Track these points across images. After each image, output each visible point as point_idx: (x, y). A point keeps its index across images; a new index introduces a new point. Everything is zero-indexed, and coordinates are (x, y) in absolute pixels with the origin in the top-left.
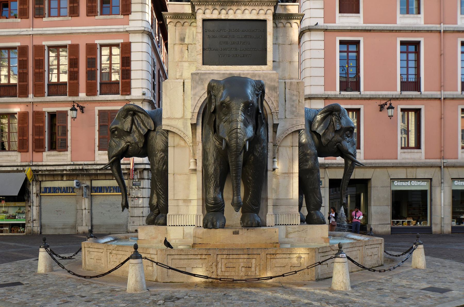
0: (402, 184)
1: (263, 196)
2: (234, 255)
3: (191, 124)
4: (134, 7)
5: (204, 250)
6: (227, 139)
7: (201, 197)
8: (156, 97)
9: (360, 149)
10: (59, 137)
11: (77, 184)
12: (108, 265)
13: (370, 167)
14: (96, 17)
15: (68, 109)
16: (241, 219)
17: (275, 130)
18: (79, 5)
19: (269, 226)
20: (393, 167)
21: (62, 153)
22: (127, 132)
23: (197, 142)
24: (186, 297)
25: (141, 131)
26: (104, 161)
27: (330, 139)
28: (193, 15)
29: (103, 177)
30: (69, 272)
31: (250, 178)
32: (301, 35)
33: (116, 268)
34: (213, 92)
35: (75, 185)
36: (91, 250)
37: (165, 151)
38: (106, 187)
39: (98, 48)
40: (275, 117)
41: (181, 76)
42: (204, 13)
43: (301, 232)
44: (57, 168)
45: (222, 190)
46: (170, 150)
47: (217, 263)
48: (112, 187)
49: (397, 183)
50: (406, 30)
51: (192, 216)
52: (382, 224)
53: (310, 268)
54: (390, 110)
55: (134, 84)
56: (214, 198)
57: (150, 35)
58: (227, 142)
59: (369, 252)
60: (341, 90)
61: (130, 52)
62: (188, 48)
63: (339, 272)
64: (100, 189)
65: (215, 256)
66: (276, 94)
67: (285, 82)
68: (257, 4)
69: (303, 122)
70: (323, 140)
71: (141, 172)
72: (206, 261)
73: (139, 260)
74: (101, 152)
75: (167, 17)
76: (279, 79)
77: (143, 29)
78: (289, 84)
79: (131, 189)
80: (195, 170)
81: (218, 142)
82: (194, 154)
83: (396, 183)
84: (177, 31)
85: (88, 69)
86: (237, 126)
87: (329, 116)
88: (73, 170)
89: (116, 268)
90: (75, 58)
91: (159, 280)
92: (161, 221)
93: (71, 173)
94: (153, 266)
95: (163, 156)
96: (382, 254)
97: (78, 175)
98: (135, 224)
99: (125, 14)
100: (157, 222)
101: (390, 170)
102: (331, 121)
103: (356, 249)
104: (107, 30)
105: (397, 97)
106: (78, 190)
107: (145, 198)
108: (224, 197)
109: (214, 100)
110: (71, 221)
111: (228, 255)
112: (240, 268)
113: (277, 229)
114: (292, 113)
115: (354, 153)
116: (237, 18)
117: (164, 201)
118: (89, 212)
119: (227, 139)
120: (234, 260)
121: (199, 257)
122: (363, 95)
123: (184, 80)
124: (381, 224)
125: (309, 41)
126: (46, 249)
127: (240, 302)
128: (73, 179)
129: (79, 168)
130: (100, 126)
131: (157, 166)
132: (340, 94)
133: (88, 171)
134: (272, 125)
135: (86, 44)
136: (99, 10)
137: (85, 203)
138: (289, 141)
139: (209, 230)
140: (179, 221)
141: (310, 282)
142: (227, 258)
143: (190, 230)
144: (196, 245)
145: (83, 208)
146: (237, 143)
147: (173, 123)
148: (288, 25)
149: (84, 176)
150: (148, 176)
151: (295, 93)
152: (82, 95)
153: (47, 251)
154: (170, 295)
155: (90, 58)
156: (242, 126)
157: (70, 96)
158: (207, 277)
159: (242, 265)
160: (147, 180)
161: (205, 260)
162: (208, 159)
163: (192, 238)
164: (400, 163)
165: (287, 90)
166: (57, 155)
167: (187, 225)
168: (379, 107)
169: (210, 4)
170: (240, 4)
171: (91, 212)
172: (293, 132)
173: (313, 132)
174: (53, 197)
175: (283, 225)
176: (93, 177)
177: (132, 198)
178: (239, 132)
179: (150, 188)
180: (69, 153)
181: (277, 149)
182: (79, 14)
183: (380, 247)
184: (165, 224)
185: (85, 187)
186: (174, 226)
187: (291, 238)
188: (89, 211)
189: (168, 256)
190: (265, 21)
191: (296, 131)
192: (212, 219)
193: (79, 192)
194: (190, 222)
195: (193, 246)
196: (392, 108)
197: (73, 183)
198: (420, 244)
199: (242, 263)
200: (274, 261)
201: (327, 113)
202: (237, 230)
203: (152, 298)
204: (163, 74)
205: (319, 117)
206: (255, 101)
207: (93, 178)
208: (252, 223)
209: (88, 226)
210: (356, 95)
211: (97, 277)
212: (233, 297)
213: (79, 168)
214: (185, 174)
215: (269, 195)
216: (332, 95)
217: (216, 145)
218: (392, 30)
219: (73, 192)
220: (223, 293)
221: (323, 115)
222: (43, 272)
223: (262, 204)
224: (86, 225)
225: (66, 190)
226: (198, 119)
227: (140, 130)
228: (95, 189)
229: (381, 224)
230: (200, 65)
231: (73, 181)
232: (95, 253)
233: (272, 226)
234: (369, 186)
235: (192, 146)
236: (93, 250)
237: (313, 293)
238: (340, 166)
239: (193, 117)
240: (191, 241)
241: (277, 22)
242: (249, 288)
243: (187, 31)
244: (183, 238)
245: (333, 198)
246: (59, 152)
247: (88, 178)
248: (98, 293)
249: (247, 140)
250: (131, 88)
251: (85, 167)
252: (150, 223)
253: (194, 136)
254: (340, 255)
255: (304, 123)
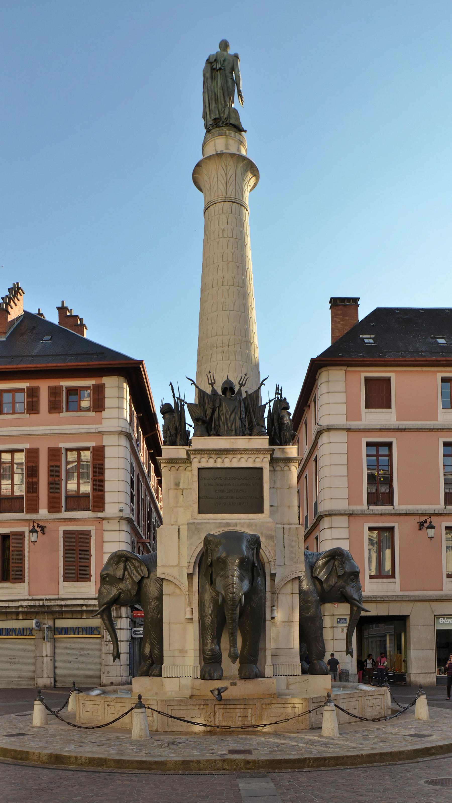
0: (449, 621)
1: (261, 646)
2: (231, 706)
3: (188, 574)
4: (108, 403)
5: (202, 701)
6: (223, 592)
7: (198, 648)
8: (135, 511)
9: (395, 578)
10: (13, 565)
11: (37, 625)
12: (106, 718)
13: (408, 600)
14: (61, 415)
15: (26, 530)
16: (239, 670)
17: (273, 578)
18: (39, 400)
19: (268, 677)
20: (436, 600)
21: (17, 585)
22: (120, 579)
23: (194, 592)
24: (187, 742)
25: (134, 578)
26: (71, 595)
27: (333, 585)
28: (188, 460)
29: (69, 616)
30: (68, 723)
31: (248, 628)
32: (318, 435)
33: (113, 722)
34: (209, 546)
35: (34, 626)
36: (86, 702)
37: (160, 599)
38: (73, 628)
39: (63, 453)
40: (273, 566)
41: (176, 521)
42: (200, 462)
43: (302, 683)
44: (11, 604)
45: (219, 642)
46: (165, 598)
47: (215, 713)
48: (81, 628)
49: (443, 621)
50: (449, 429)
51: (188, 666)
52: (425, 673)
53: (302, 716)
54: (431, 530)
55: (108, 498)
56: (211, 649)
57: (129, 436)
58: (223, 596)
59: (370, 703)
60: (370, 503)
61: (103, 458)
62: (183, 492)
63: (328, 719)
64: (66, 631)
65: (213, 706)
66: (273, 543)
67: (284, 528)
68: (252, 453)
69: (303, 569)
70: (325, 586)
71: (119, 609)
72: (204, 711)
73: (143, 710)
74: (66, 583)
75: (162, 462)
76: (277, 524)
77: (120, 429)
78: (288, 530)
79: (105, 631)
80: (192, 619)
81: (214, 593)
82: (190, 603)
83: (441, 620)
84: (172, 476)
85: (51, 479)
86: (233, 582)
87: (332, 561)
88: (31, 606)
89: (113, 722)
90: (34, 465)
91: (159, 730)
92: (156, 672)
93: (29, 610)
94: (153, 717)
95: (157, 605)
96: (385, 705)
97: (37, 613)
98: (110, 674)
99: (97, 410)
100: (151, 674)
101: (434, 604)
102: (333, 565)
103: (354, 699)
104: (74, 431)
105: (440, 512)
106: (37, 632)
107: (122, 641)
108: (221, 647)
109: (210, 554)
110: (28, 671)
111: (225, 705)
112: (237, 717)
113: (274, 680)
114: (292, 559)
115: (359, 598)
116: (233, 466)
117: (158, 651)
118: (51, 660)
119: (223, 594)
120: (231, 711)
121: (198, 707)
122: (397, 510)
123: (179, 527)
124: (424, 673)
125: (329, 443)
126: (42, 701)
127: (235, 745)
128: (31, 617)
129: (39, 604)
130: (66, 551)
131: (151, 614)
132: (368, 509)
133: (50, 608)
134: (269, 574)
135: (48, 448)
136: (64, 406)
137: (47, 648)
138: (288, 588)
139: (206, 681)
140: (175, 673)
141: (304, 730)
142: (225, 708)
143: (188, 682)
144: (194, 697)
145: (44, 654)
146: (233, 597)
147: (167, 570)
148: (286, 468)
149: (46, 614)
150: (127, 613)
151: (294, 539)
152: (43, 512)
153: (43, 704)
154: (173, 741)
155: (52, 466)
156: (238, 581)
157: (27, 512)
158: (205, 725)
159: (239, 714)
160: (125, 619)
161: (203, 710)
162: (204, 610)
163: (190, 690)
164: (446, 596)
165: (286, 536)
166: (11, 588)
167: (183, 677)
168: (417, 526)
169: (206, 453)
170: (236, 453)
171: (55, 660)
172: (292, 579)
173: (315, 579)
174: (6, 641)
175: (284, 675)
176: (57, 615)
177: (106, 641)
178: (235, 587)
179: (129, 629)
180: (26, 585)
181: (276, 597)
182: (39, 410)
183: (383, 698)
184: (160, 675)
185: (47, 627)
186: (170, 677)
187: (292, 689)
188: (52, 658)
189: (168, 706)
190: (261, 469)
191: (295, 578)
192: (210, 670)
193: (40, 635)
194: (186, 674)
195: (190, 698)
196: (433, 527)
197: (33, 623)
198: (423, 694)
199: (238, 713)
200: (269, 711)
201: (328, 558)
202: (235, 681)
203: (156, 743)
204: (143, 478)
205: (320, 562)
206: (250, 556)
207: (57, 617)
208: (250, 675)
209: (51, 678)
210: (388, 510)
211: (100, 727)
212: (230, 742)
213: (39, 604)
214: (181, 624)
215: (268, 646)
216: (358, 511)
217: (213, 597)
218: (433, 429)
219: (31, 634)
220: (220, 739)
221: (324, 560)
222: (39, 725)
223: (261, 654)
224: (48, 677)
225: (21, 631)
226: (194, 569)
227: (133, 577)
228: (59, 630)
229: (424, 673)
230: (196, 514)
231: (31, 621)
232: (91, 706)
233: (270, 677)
234: (407, 624)
235: (189, 594)
236: (89, 702)
237: (303, 738)
238: (369, 599)
239: (189, 567)
240: (188, 693)
241: (275, 466)
242: (244, 735)
243: (182, 475)
244: (180, 691)
245: (376, 635)
246: (14, 584)
247: (51, 617)
248: (106, 740)
249: (242, 595)
250: (105, 503)
251: (47, 603)
252: (143, 675)
253: (190, 585)
254: (329, 704)
255: (304, 570)
